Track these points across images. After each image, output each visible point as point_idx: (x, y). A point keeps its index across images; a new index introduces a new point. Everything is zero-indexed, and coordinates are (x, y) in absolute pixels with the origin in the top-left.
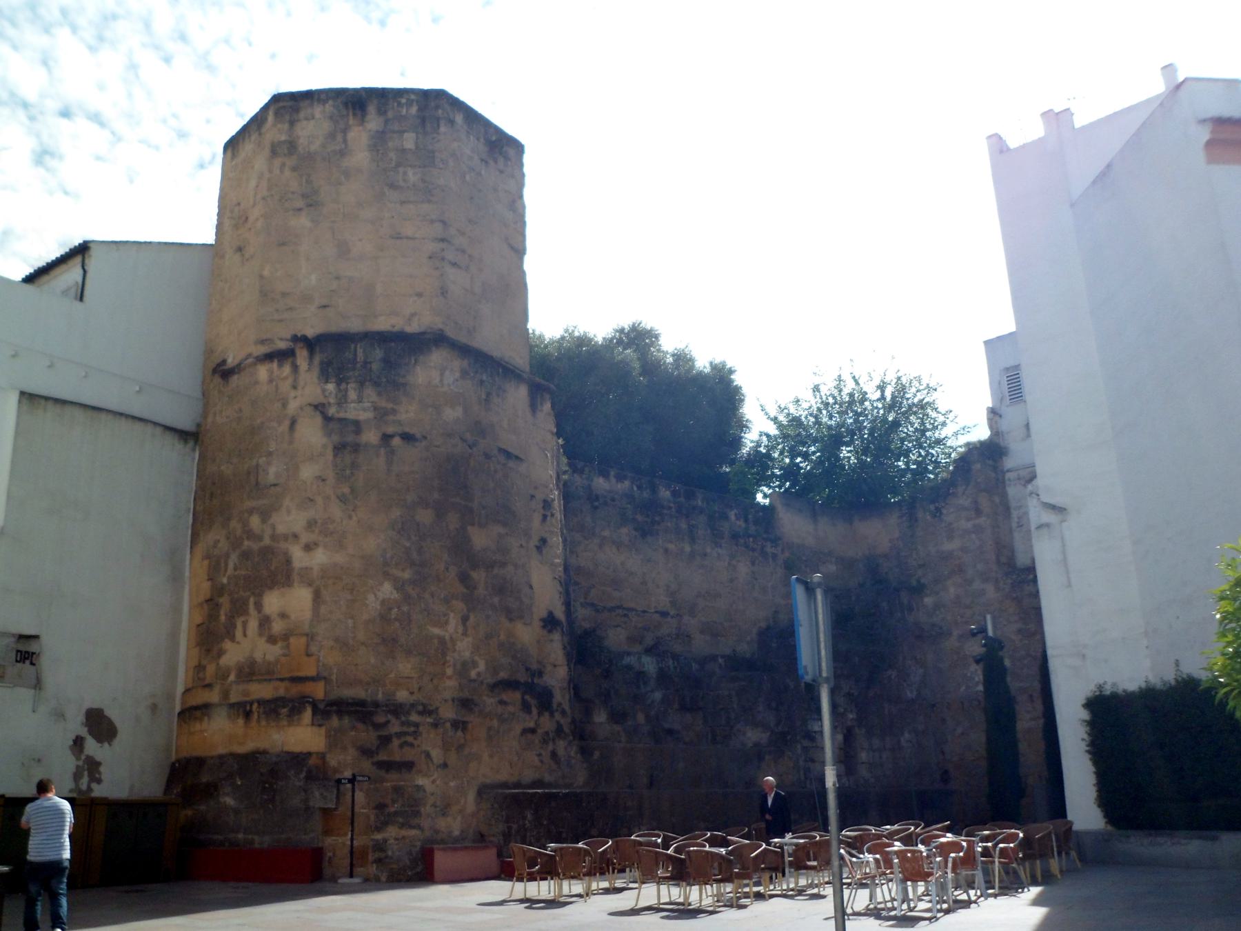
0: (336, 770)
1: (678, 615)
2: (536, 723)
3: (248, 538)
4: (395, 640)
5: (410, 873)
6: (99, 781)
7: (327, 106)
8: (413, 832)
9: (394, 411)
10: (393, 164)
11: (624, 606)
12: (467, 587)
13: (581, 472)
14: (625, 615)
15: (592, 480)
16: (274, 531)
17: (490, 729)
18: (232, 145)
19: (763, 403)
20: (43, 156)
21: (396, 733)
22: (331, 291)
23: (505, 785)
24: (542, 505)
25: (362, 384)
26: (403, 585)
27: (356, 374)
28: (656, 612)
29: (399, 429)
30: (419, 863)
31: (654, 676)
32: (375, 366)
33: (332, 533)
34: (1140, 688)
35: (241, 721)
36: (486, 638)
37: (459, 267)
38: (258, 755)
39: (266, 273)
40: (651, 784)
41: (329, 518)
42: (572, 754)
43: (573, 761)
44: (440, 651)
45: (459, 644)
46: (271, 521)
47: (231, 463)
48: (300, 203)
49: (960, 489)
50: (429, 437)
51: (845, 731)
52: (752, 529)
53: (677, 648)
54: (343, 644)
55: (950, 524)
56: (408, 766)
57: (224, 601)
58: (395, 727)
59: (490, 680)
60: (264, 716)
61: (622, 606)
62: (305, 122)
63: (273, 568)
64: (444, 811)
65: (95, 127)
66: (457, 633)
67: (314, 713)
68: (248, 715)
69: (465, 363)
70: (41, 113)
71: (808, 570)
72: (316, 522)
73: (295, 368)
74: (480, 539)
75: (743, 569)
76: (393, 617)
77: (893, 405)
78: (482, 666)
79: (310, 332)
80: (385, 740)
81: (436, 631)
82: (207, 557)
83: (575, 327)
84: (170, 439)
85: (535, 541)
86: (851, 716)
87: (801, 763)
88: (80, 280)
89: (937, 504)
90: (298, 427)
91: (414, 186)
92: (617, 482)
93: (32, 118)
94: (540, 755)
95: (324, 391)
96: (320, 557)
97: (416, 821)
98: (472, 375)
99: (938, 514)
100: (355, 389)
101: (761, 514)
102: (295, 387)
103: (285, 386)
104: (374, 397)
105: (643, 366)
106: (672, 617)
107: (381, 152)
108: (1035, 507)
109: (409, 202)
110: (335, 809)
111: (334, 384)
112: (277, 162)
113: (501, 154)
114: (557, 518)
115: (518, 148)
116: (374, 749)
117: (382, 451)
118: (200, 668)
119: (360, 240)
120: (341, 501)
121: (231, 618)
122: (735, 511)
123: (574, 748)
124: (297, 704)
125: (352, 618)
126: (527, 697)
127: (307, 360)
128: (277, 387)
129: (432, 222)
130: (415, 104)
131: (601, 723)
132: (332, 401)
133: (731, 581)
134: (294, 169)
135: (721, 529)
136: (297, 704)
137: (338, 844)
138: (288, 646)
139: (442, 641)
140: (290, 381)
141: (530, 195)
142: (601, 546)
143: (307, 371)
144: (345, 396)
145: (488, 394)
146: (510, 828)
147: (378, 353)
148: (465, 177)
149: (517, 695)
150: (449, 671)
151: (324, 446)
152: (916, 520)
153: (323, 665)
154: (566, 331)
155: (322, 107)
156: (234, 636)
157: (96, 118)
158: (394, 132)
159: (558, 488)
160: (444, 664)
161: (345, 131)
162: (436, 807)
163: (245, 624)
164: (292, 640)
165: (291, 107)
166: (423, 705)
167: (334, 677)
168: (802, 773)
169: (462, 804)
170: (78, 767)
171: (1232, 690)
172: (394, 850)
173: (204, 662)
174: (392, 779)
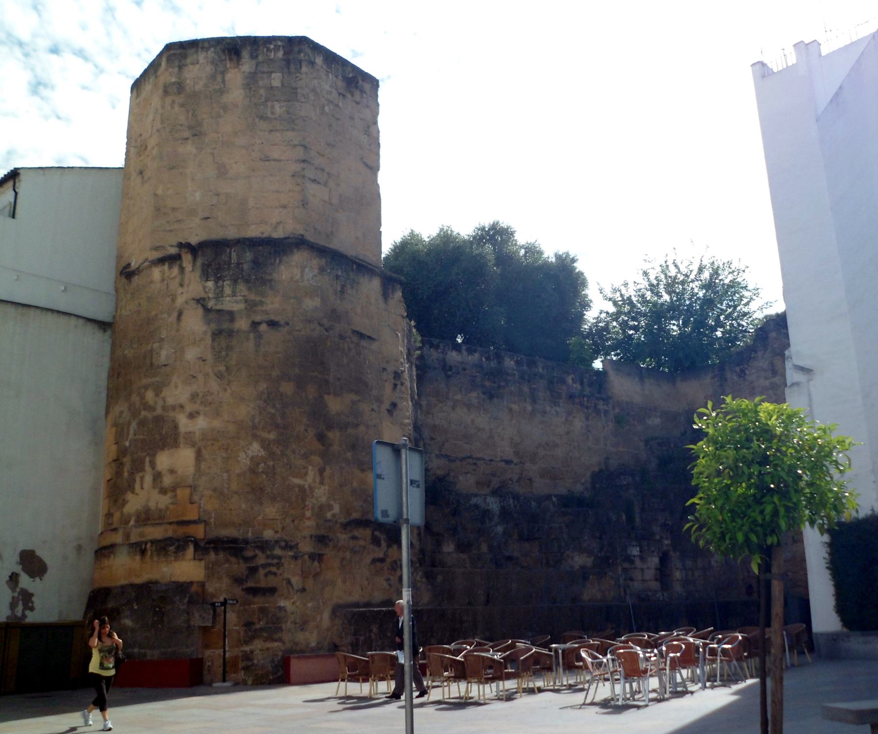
0: (213, 596)
1: (521, 462)
2: (385, 554)
3: (144, 409)
4: (262, 490)
5: (271, 677)
6: (32, 609)
7: (209, 52)
8: (276, 644)
9: (261, 303)
10: (263, 100)
11: (474, 456)
12: (323, 445)
13: (437, 347)
14: (475, 464)
15: (446, 354)
16: (165, 403)
17: (343, 559)
18: (137, 86)
19: (602, 286)
20: (37, 86)
21: (262, 565)
22: (212, 205)
23: (357, 605)
24: (393, 376)
25: (235, 281)
26: (268, 445)
27: (231, 273)
28: (502, 461)
29: (265, 318)
30: (280, 669)
31: (498, 513)
32: (245, 267)
33: (210, 404)
34: (866, 516)
35: (138, 558)
36: (340, 485)
37: (319, 183)
38: (151, 585)
39: (159, 192)
40: (487, 602)
41: (208, 392)
42: (418, 578)
43: (419, 584)
44: (300, 497)
45: (317, 490)
46: (163, 394)
47: (132, 348)
48: (187, 134)
49: (760, 354)
50: (291, 323)
51: (661, 555)
52: (587, 391)
53: (520, 490)
54: (220, 493)
55: (752, 383)
56: (272, 591)
57: (127, 460)
58: (261, 560)
59: (343, 520)
60: (155, 553)
61: (472, 456)
62: (191, 67)
63: (164, 432)
64: (303, 625)
65: (80, 61)
66: (315, 482)
67: (196, 550)
68: (143, 552)
69: (323, 262)
70: (35, 50)
71: (636, 423)
72: (198, 395)
73: (182, 269)
74: (335, 405)
75: (578, 423)
76: (260, 470)
77: (709, 286)
78: (336, 509)
79: (194, 240)
80: (253, 570)
81: (297, 481)
82: (115, 425)
83: (449, 227)
84: (90, 328)
85: (386, 405)
86: (666, 542)
87: (621, 581)
88: (12, 200)
89: (741, 367)
90: (183, 317)
91: (280, 116)
92: (468, 355)
93: (26, 55)
94: (388, 580)
95: (204, 288)
96: (201, 423)
97: (278, 635)
98: (329, 271)
99: (742, 375)
100: (229, 286)
101: (595, 378)
102: (181, 285)
103: (174, 285)
104: (245, 292)
105: (497, 259)
106: (516, 464)
107: (253, 89)
108: (790, 369)
109: (277, 130)
110: (213, 627)
111: (213, 282)
112: (168, 100)
113: (357, 88)
114: (406, 386)
115: (374, 83)
116: (244, 577)
117: (252, 335)
118: (109, 515)
119: (236, 163)
120: (218, 377)
121: (132, 474)
122: (572, 376)
123: (420, 574)
124: (181, 543)
125: (227, 471)
126: (377, 533)
127: (192, 263)
128: (167, 285)
129: (295, 146)
130: (281, 48)
131: (449, 553)
132: (211, 296)
133: (568, 433)
134: (182, 105)
135: (559, 391)
136: (181, 543)
137: (213, 656)
138: (175, 496)
139: (302, 489)
140: (177, 281)
141: (385, 122)
142: (453, 408)
143: (191, 272)
144: (222, 291)
145: (343, 287)
146: (357, 640)
147: (249, 256)
148: (324, 108)
149: (368, 532)
150: (308, 514)
151: (205, 333)
152: (726, 380)
153: (204, 511)
154: (441, 230)
155: (205, 53)
156: (134, 488)
157: (80, 53)
158: (264, 73)
159: (409, 360)
160: (303, 508)
161: (223, 73)
162: (295, 623)
163: (142, 478)
164: (179, 491)
165: (180, 54)
166: (286, 541)
167: (212, 520)
168: (622, 589)
169: (318, 621)
170: (13, 598)
171: (693, 526)
172: (259, 658)
173: (112, 511)
174: (259, 602)
